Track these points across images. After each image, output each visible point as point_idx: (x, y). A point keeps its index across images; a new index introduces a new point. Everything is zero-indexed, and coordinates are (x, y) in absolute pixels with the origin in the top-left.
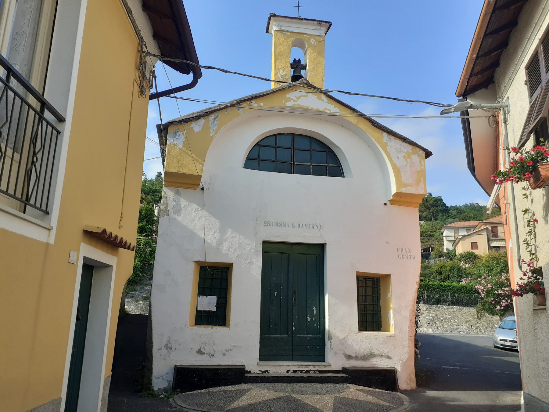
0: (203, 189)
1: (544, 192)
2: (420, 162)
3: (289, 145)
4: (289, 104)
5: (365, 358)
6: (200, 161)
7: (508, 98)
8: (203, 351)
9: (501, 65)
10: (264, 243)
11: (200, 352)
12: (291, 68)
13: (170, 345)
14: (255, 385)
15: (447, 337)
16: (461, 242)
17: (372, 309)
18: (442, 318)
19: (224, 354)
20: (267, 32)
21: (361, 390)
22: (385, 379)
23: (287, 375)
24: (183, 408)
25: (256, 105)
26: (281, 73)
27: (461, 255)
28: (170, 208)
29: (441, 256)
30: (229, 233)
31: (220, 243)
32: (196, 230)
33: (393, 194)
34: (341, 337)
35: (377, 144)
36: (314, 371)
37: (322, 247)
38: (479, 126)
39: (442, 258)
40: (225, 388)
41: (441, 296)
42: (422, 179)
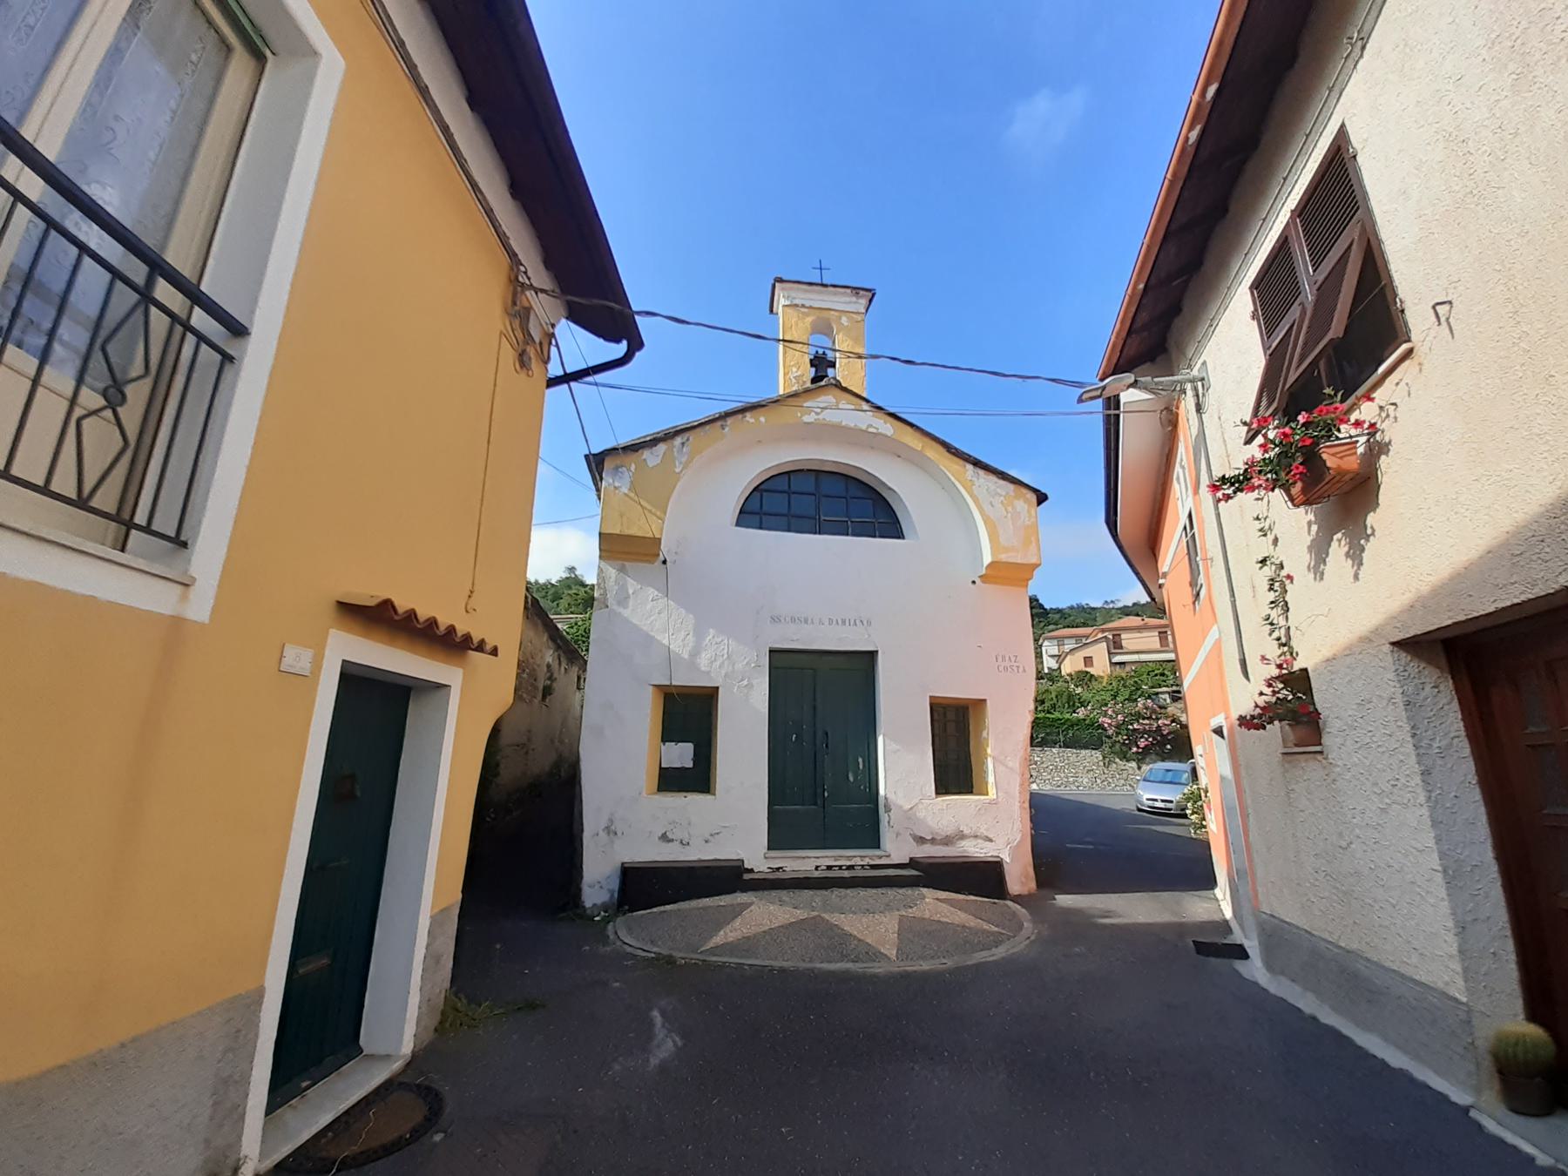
0: (664, 562)
1: (1311, 517)
3: (811, 489)
4: (806, 419)
5: (947, 841)
7: (1204, 363)
8: (670, 836)
9: (1185, 310)
11: (664, 838)
14: (760, 893)
22: (981, 878)
23: (817, 874)
31: (695, 653)
37: (871, 656)
38: (1136, 439)
40: (707, 901)
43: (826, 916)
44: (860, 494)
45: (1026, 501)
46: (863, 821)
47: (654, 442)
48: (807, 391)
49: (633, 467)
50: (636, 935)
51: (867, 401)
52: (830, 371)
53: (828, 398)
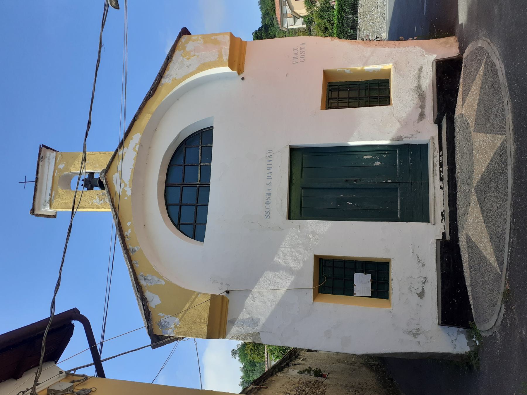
0: (228, 292)
2: (194, 41)
3: (179, 189)
4: (129, 192)
5: (422, 97)
6: (194, 297)
8: (419, 291)
10: (290, 218)
12: (93, 189)
13: (414, 331)
14: (460, 228)
15: (391, 17)
16: (295, 11)
17: (364, 91)
18: (371, 24)
19: (424, 265)
20: (55, 216)
21: (464, 101)
22: (448, 73)
23: (446, 188)
24: (497, 325)
25: (130, 231)
26: (96, 201)
27: (308, 10)
28: (251, 331)
29: (309, 29)
30: (279, 260)
31: (290, 270)
32: (276, 295)
33: (231, 71)
34: (398, 125)
35: (174, 90)
36: (440, 156)
37: (293, 150)
39: (312, 29)
40: (465, 265)
41: (348, 26)
42: (213, 38)
43: (474, 185)
44: (182, 157)
45: (187, 42)
46: (409, 156)
47: (143, 300)
48: (109, 193)
49: (161, 314)
50: (489, 316)
51: (117, 151)
52: (96, 176)
53: (115, 178)
